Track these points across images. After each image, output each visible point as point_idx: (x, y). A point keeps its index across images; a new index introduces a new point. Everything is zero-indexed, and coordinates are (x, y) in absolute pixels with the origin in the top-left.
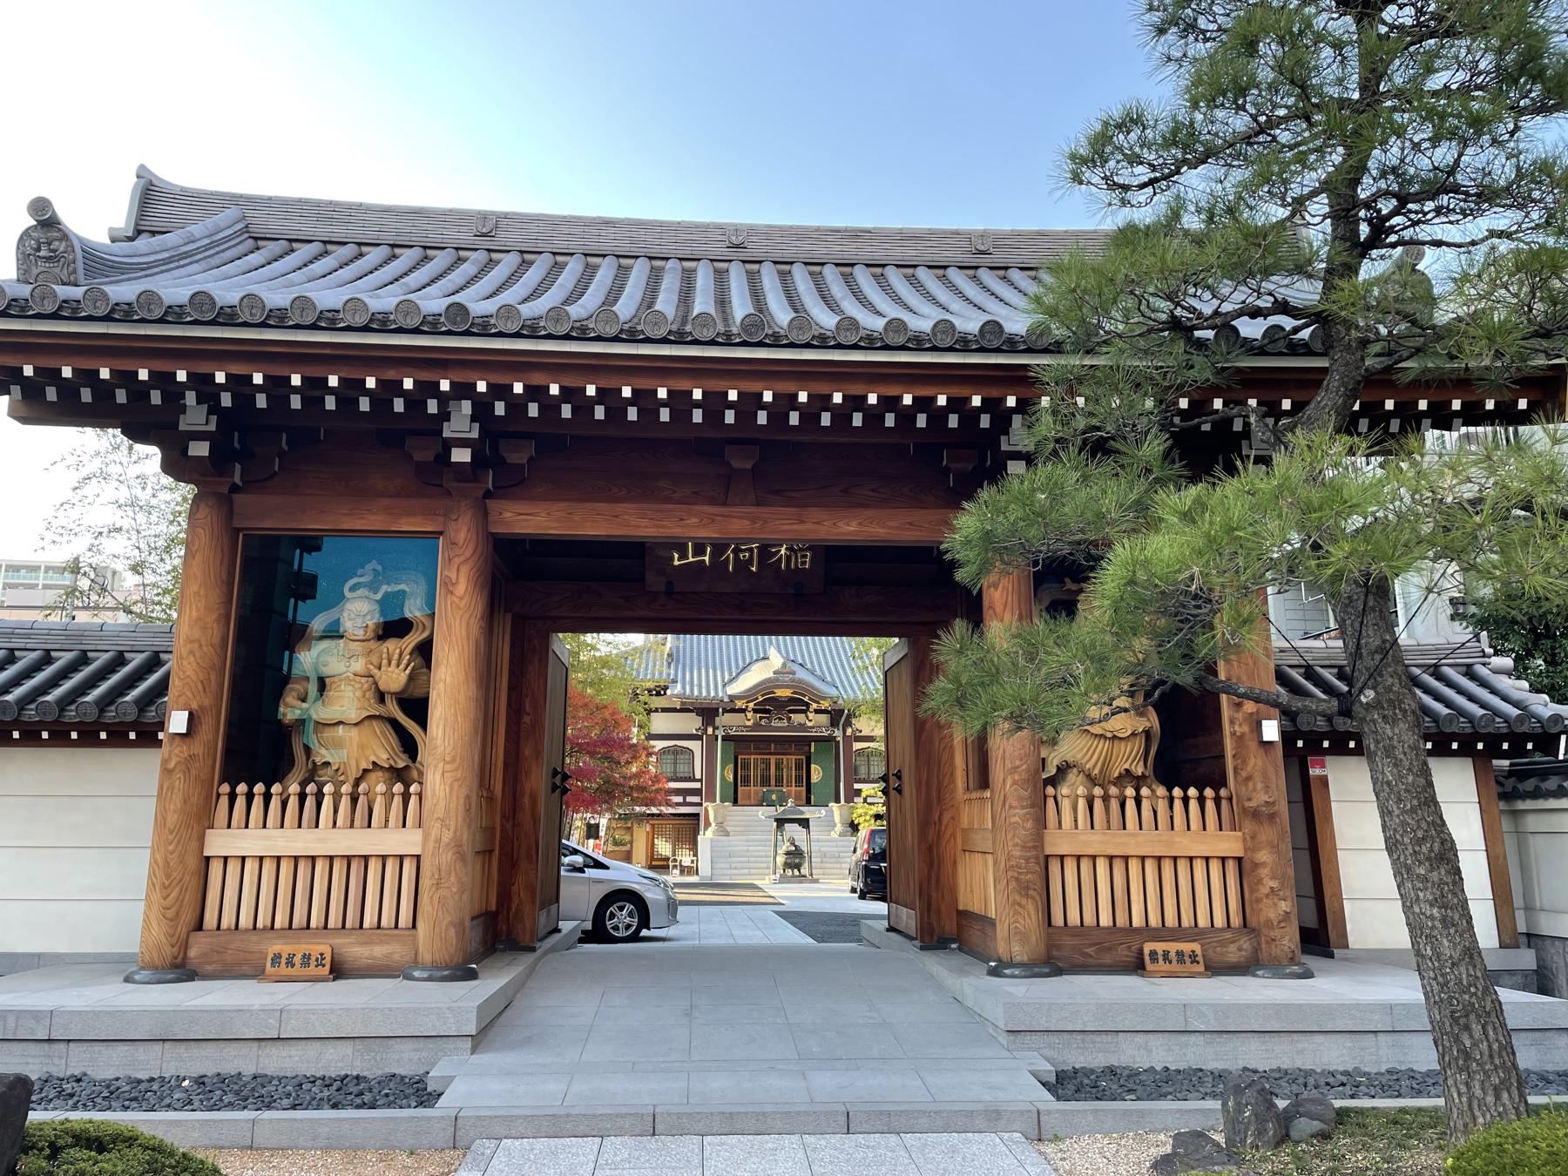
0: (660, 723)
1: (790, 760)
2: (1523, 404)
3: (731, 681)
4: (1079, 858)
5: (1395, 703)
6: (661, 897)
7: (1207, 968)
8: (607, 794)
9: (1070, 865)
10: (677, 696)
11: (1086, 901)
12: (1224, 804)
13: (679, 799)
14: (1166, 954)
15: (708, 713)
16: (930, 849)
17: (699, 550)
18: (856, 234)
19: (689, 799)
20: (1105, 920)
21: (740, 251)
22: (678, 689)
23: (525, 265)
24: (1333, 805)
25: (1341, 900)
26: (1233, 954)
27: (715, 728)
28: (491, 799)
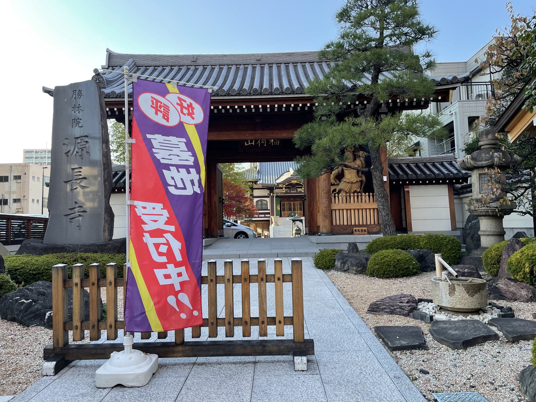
0: (256, 193)
1: (298, 203)
2: (440, 98)
3: (278, 179)
4: (339, 210)
6: (252, 233)
8: (240, 211)
9: (337, 212)
13: (263, 216)
14: (358, 230)
15: (271, 189)
17: (251, 142)
18: (290, 54)
19: (266, 216)
20: (345, 224)
21: (261, 62)
22: (261, 182)
24: (249, 163)
26: (375, 230)
27: (273, 193)
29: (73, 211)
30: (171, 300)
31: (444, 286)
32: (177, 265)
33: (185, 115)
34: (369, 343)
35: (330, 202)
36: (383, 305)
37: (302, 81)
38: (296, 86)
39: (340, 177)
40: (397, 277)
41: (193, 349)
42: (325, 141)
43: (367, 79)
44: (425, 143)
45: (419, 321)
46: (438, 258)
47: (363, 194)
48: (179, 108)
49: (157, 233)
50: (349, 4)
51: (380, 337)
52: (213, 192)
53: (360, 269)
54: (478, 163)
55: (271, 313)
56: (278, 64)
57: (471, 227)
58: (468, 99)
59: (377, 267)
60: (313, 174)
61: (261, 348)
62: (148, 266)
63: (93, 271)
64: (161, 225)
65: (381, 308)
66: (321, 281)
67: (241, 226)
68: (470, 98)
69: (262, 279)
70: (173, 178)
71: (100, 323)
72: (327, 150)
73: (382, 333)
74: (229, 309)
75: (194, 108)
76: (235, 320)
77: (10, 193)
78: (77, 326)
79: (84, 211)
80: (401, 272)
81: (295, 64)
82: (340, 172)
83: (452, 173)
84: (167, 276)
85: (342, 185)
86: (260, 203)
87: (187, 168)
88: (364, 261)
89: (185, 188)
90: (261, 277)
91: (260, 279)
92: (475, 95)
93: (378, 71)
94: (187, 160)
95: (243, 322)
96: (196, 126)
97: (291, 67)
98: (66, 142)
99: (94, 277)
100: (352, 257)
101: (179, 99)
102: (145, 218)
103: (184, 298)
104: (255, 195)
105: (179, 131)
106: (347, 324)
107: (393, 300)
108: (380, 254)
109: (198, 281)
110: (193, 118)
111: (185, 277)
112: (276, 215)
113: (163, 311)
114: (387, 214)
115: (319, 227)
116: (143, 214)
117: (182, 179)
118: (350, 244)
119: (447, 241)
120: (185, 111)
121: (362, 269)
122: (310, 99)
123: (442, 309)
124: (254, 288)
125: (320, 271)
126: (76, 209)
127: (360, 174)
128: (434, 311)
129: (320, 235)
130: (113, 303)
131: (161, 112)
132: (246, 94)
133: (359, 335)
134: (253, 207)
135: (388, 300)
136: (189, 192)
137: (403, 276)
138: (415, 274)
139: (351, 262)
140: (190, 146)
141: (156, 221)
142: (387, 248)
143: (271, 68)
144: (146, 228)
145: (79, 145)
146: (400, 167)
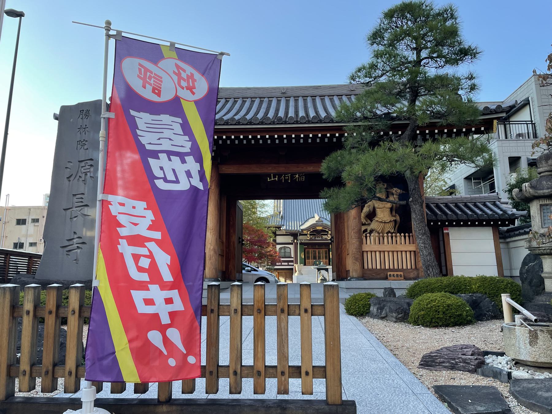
0: (279, 239)
1: (323, 251)
2: (483, 129)
3: (302, 225)
4: (371, 252)
5: (416, 201)
7: (404, 278)
8: (261, 256)
10: (284, 230)
11: (373, 262)
12: (411, 237)
13: (287, 264)
14: (393, 275)
15: (295, 235)
16: (339, 255)
17: (274, 177)
19: (290, 264)
20: (378, 267)
21: (285, 95)
22: (284, 228)
23: (227, 102)
24: (273, 201)
25: (452, 266)
26: (412, 275)
27: (297, 240)
28: (222, 243)
29: (71, 243)
30: (155, 337)
31: (522, 333)
32: (164, 286)
33: (183, 88)
34: (431, 409)
35: (361, 243)
36: (440, 357)
37: (329, 110)
38: (323, 114)
39: (371, 215)
40: (447, 325)
41: (182, 410)
42: (357, 169)
43: (403, 105)
44: (461, 186)
45: (491, 379)
46: (506, 299)
47: (398, 234)
48: (175, 78)
49: (137, 240)
50: (382, 25)
51: (444, 400)
52: (232, 231)
53: (400, 316)
54: (539, 192)
55: (295, 360)
56: (305, 97)
57: (528, 271)
58: (506, 138)
59: (423, 313)
60: (343, 207)
61: (279, 411)
62: (123, 286)
63: (52, 294)
64: (143, 230)
65: (438, 361)
66: (355, 328)
67: (262, 271)
68: (509, 135)
69: (282, 311)
70: (162, 168)
71: (57, 368)
72: (360, 180)
73: (443, 393)
74: (236, 352)
75: (196, 81)
76: (243, 368)
77: (26, 236)
78: (25, 371)
79: (83, 243)
80: (452, 320)
81: (322, 97)
82: (372, 210)
83: (497, 213)
84: (149, 302)
85: (374, 225)
86: (283, 251)
87: (182, 156)
88: (405, 306)
89: (177, 181)
90: (281, 307)
91: (279, 311)
92: (515, 135)
93: (415, 95)
94: (182, 146)
95: (255, 371)
96: (197, 102)
97: (318, 100)
98: (69, 165)
99: (51, 303)
100: (390, 301)
101: (177, 66)
102: (122, 219)
103: (174, 335)
104: (278, 241)
105: (174, 107)
106: (395, 381)
107: (452, 351)
108: (426, 297)
109: (196, 312)
110: (193, 93)
111: (178, 305)
112: (300, 264)
113: (143, 353)
114: (430, 254)
115: (348, 272)
116: (119, 213)
117: (174, 170)
118: (385, 289)
119: (505, 283)
120: (184, 84)
121: (403, 316)
122: (339, 129)
123: (518, 363)
124: (271, 322)
125: (353, 318)
126: (75, 241)
127: (394, 213)
128: (509, 366)
129: (349, 280)
130: (75, 340)
131: (150, 84)
132: (269, 122)
133: (415, 397)
134: (276, 252)
135: (446, 352)
136: (184, 185)
137: (455, 324)
138: (468, 323)
139: (390, 308)
140: (186, 129)
141: (136, 224)
142: (432, 291)
143: (296, 101)
144: (123, 232)
145: (82, 169)
146: (438, 206)
